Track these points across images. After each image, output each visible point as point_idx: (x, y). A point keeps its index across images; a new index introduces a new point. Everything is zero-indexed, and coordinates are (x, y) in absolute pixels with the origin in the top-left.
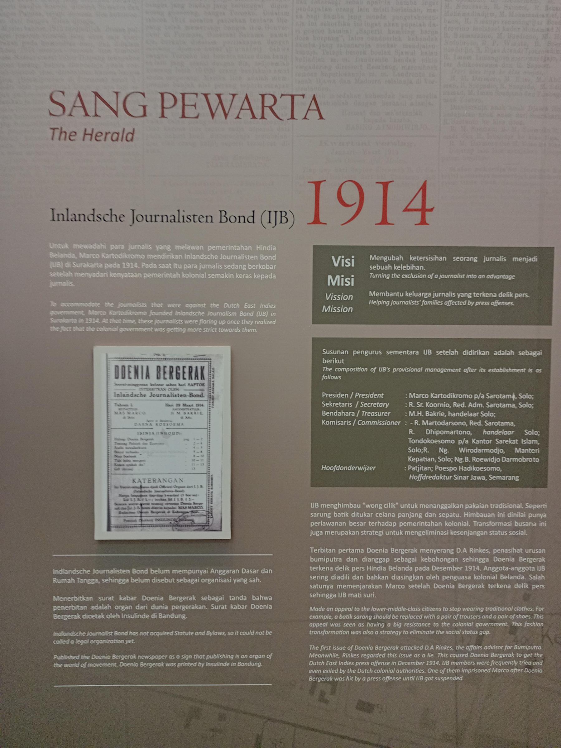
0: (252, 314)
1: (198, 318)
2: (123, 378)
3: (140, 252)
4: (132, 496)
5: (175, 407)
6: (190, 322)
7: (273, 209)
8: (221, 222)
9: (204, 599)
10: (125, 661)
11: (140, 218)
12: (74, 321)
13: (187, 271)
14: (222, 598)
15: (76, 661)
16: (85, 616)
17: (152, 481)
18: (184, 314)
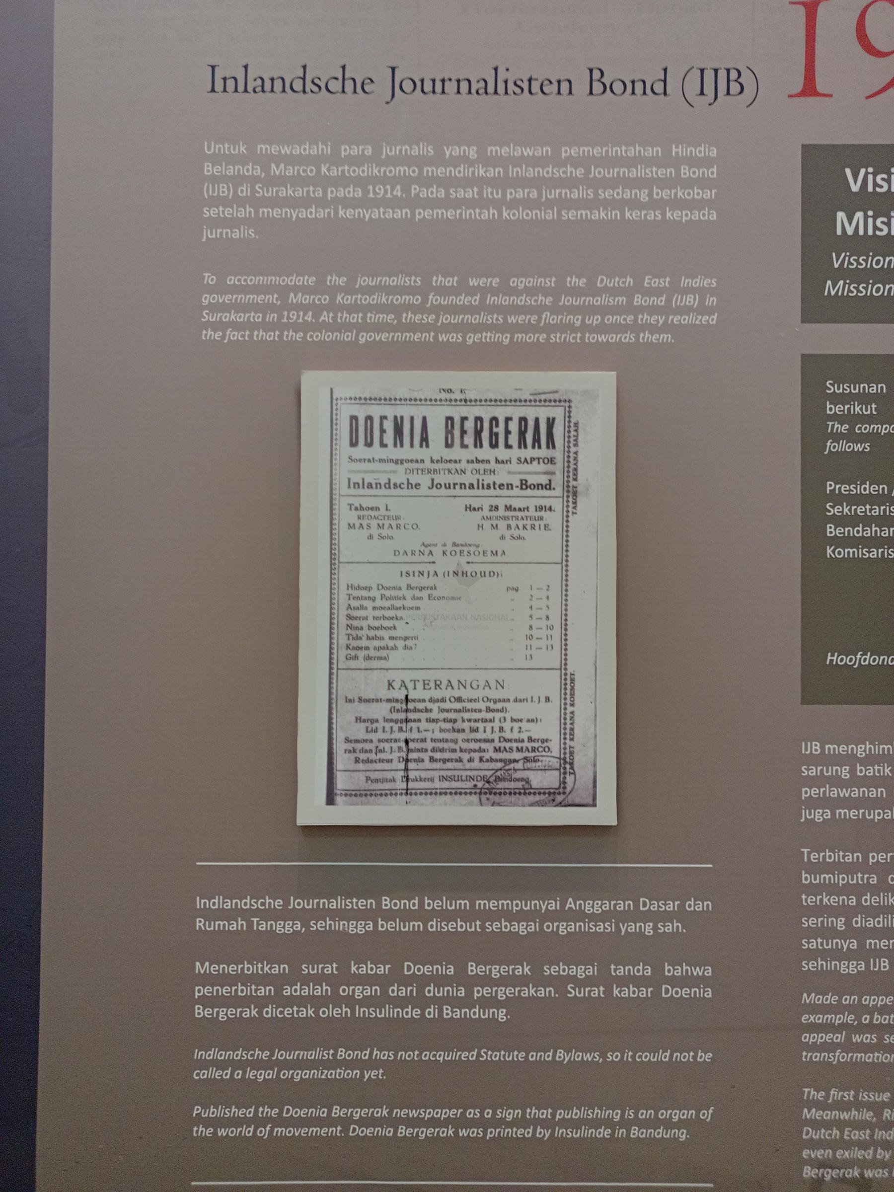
0: (662, 301)
1: (539, 310)
2: (369, 444)
3: (409, 160)
4: (386, 720)
5: (486, 512)
6: (520, 319)
7: (709, 65)
8: (591, 93)
9: (550, 970)
10: (363, 1122)
11: (408, 86)
12: (258, 318)
13: (514, 204)
14: (591, 971)
15: (246, 1121)
16: (269, 1012)
17: (432, 685)
18: (505, 300)
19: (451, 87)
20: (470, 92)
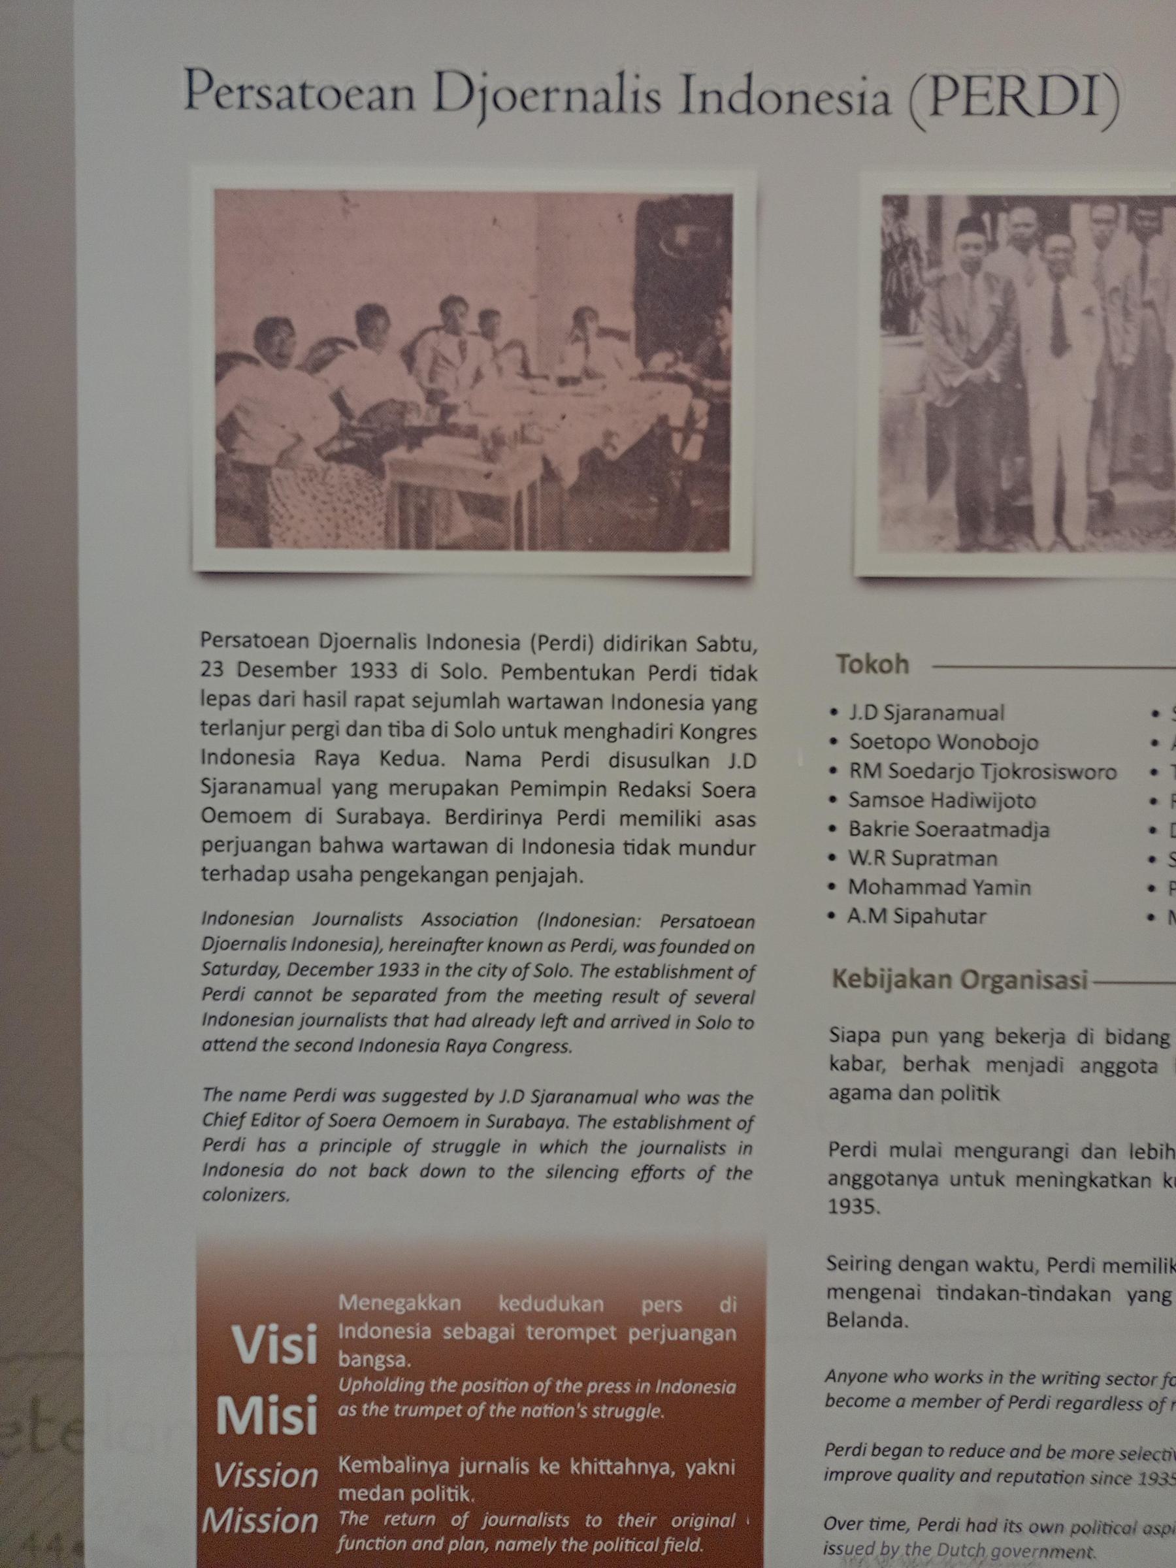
8: (440, 107)
19: (558, 101)
20: (584, 108)
